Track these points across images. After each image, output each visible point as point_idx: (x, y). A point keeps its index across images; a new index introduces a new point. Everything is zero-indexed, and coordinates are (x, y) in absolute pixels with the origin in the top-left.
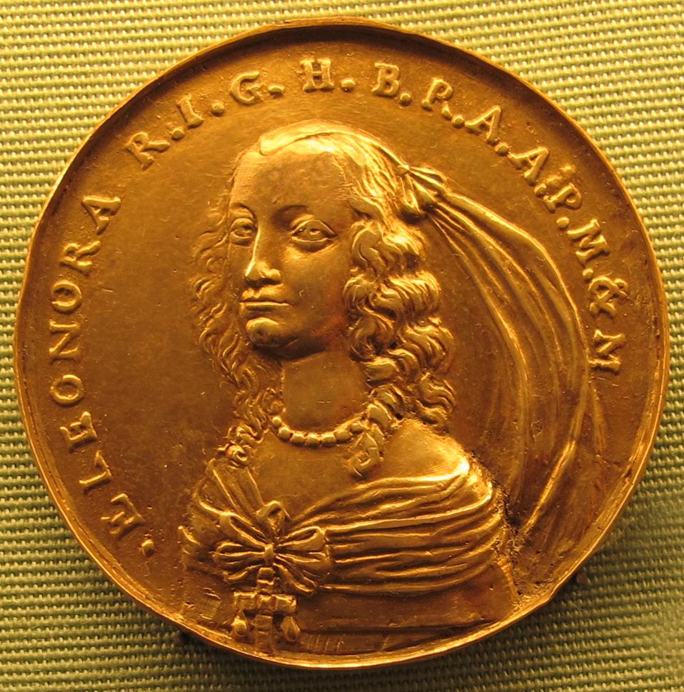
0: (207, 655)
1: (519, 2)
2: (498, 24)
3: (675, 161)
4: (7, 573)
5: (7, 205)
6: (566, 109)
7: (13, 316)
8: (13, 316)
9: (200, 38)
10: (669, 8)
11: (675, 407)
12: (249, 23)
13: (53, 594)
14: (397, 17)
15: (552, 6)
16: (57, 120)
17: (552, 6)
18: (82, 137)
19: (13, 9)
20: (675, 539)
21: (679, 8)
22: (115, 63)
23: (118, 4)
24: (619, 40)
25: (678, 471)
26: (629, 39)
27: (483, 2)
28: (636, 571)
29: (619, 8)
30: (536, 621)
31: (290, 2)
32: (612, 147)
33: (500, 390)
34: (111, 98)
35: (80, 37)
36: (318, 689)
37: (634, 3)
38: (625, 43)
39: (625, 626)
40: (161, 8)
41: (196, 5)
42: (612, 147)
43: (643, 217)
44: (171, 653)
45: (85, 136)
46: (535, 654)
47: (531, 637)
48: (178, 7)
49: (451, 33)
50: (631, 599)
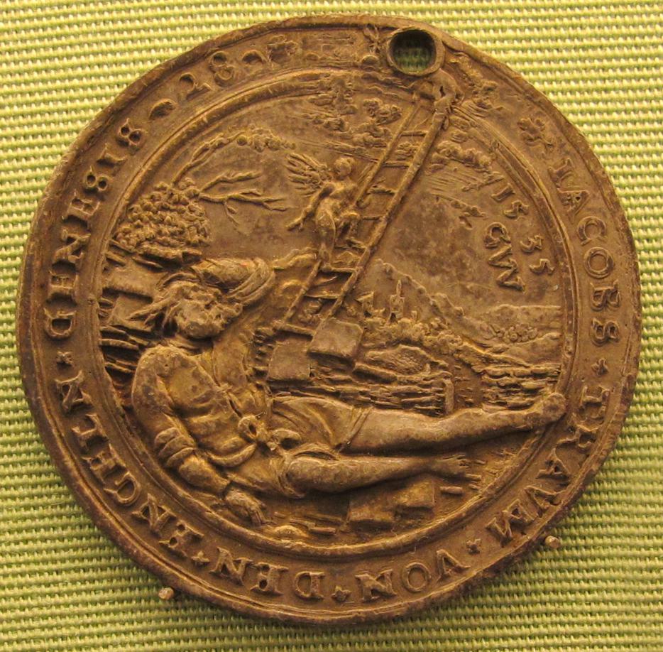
1: (493, 2)
3: (655, 165)
4: (7, 487)
5: (7, 138)
7: (13, 304)
8: (52, 475)
10: (211, 8)
12: (272, 12)
16: (29, 31)
18: (66, 144)
19: (168, 11)
21: (656, 8)
23: (458, 4)
24: (560, 18)
25: (636, 430)
26: (570, 17)
27: (81, 3)
29: (545, 8)
32: (590, 123)
33: (345, 249)
34: (108, 90)
35: (139, 44)
38: (566, 21)
40: (554, 8)
41: (632, 5)
42: (590, 123)
48: (597, 6)
50: (586, 543)
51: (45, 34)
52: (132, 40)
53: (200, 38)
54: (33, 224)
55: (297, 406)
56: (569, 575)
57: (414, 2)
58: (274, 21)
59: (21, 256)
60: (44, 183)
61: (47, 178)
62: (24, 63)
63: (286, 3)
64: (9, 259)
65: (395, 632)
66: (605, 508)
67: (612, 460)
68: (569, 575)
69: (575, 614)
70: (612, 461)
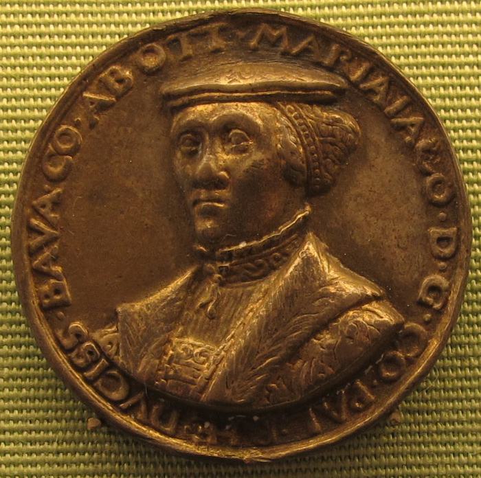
0: (150, 456)
2: (383, 25)
6: (427, 98)
9: (52, 27)
10: (86, 7)
11: (469, 342)
12: (172, 12)
13: (21, 431)
14: (389, 50)
15: (346, 5)
17: (346, 5)
20: (453, 424)
22: (455, 35)
27: (403, 2)
28: (419, 444)
30: (373, 451)
31: (225, 2)
32: (446, 109)
34: (143, 17)
36: (230, 474)
37: (310, 3)
39: (439, 454)
43: (470, 193)
44: (111, 463)
45: (28, 150)
46: (391, 451)
47: (350, 469)
49: (362, 30)
51: (38, 9)
52: (136, 13)
53: (117, 36)
54: (19, 185)
55: (255, 285)
56: (429, 418)
57: (217, 2)
58: (245, 13)
59: (14, 193)
60: (66, 81)
61: (23, 151)
62: (90, 48)
63: (169, 3)
64: (12, 422)
65: (458, 15)
66: (448, 374)
67: (454, 337)
68: (429, 418)
69: (429, 412)
70: (454, 337)
